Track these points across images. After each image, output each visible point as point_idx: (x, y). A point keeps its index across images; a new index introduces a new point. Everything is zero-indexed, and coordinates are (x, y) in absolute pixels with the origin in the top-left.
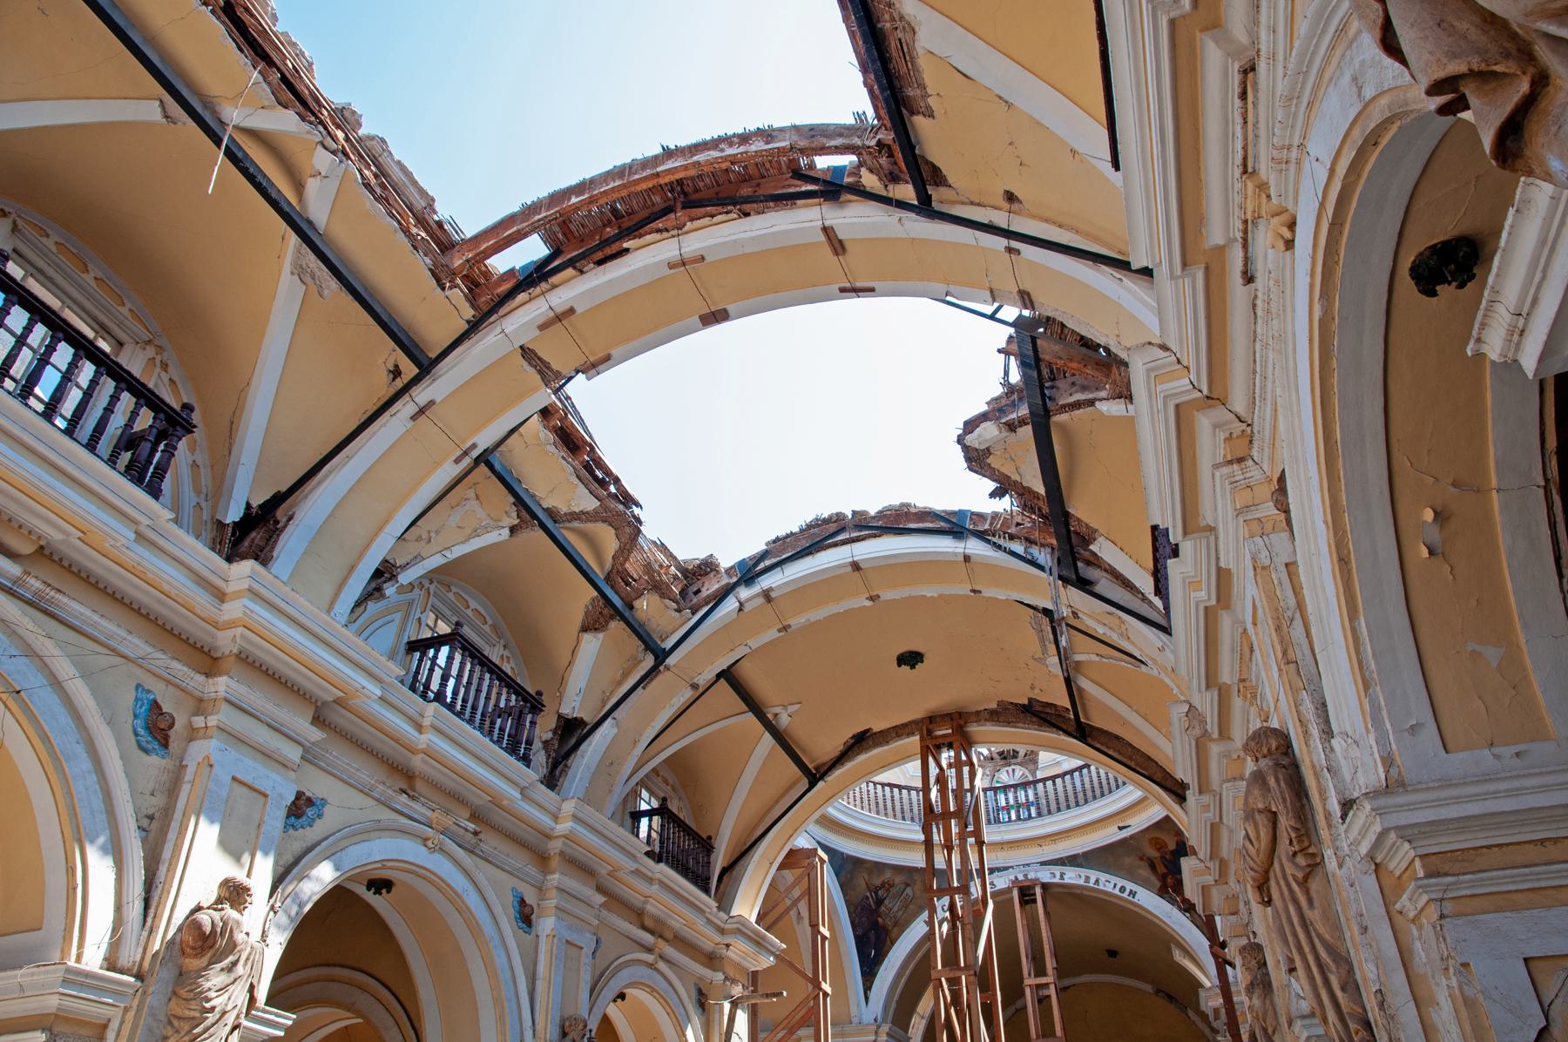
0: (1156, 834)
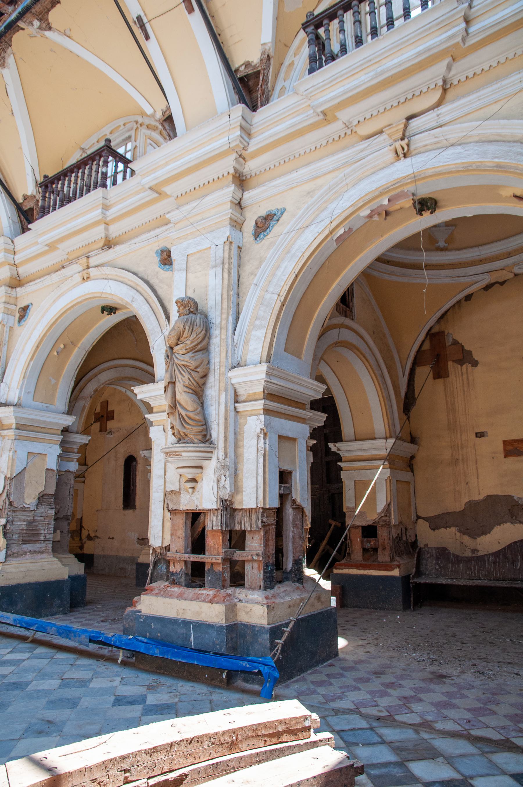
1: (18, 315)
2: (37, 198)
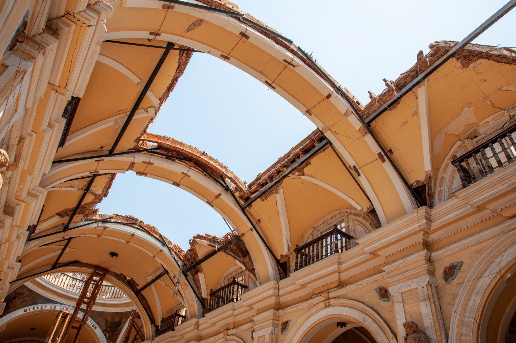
1: (280, 327)
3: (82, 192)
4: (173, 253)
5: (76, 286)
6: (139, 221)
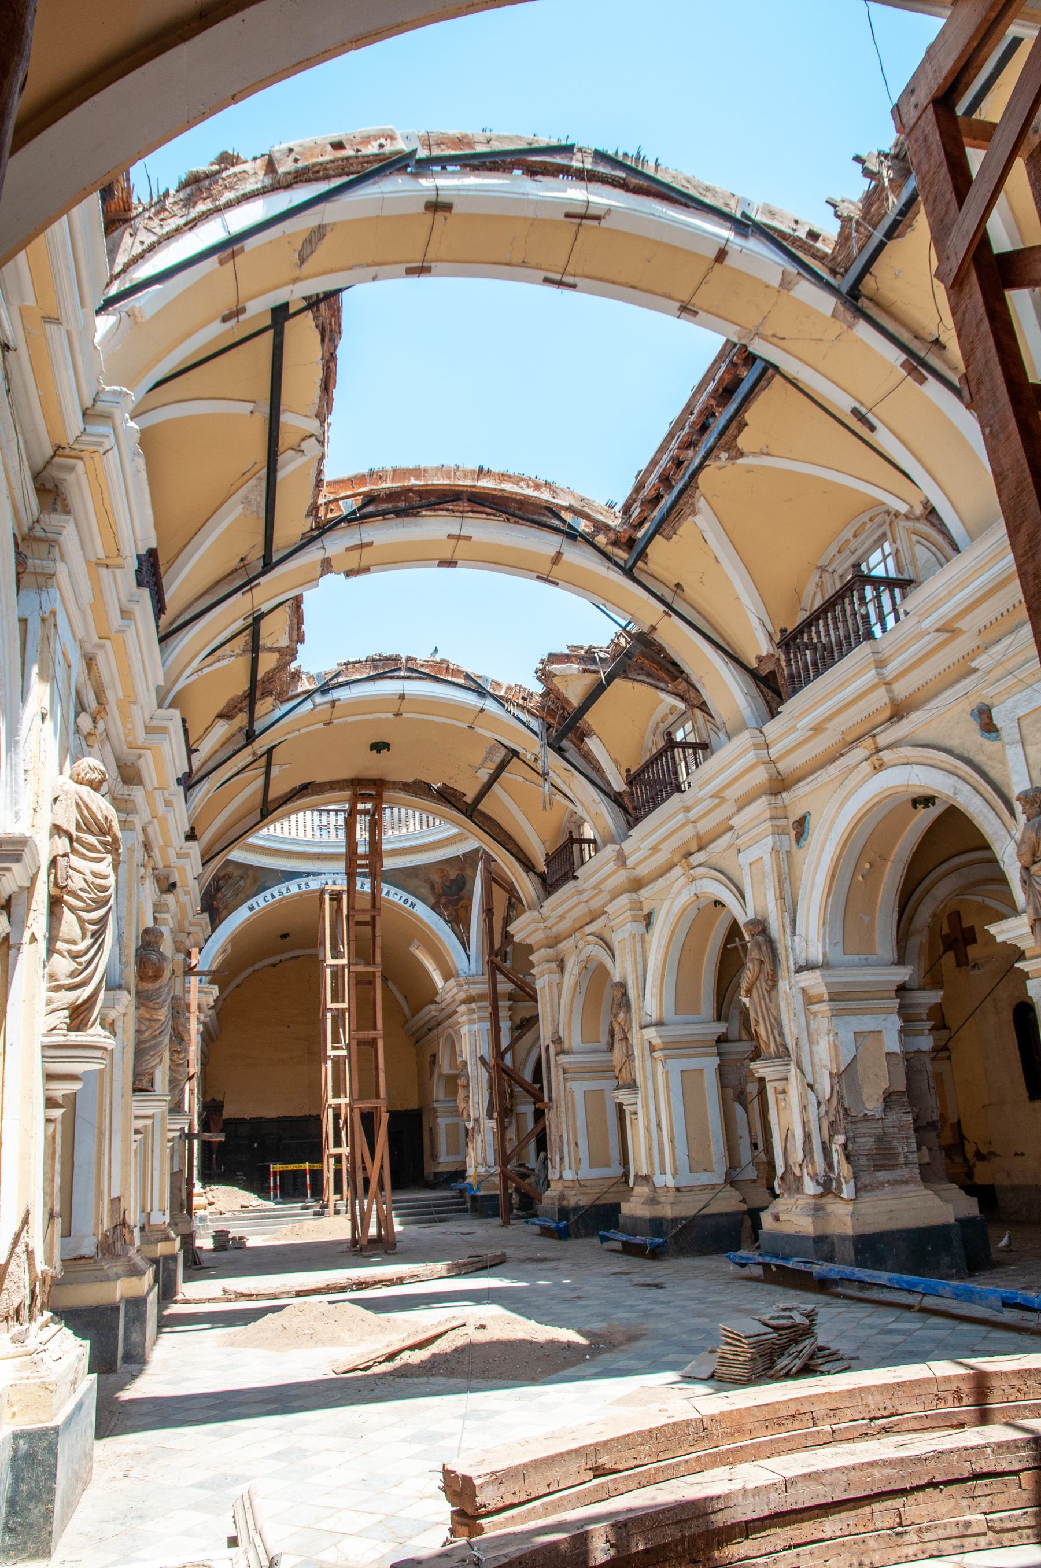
0: (447, 868)
1: (793, 833)
2: (777, 656)
3: (249, 655)
4: (511, 708)
5: (332, 827)
6: (403, 660)
